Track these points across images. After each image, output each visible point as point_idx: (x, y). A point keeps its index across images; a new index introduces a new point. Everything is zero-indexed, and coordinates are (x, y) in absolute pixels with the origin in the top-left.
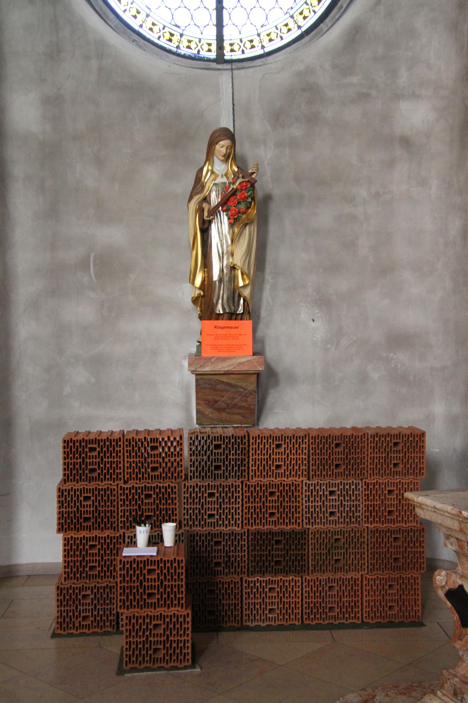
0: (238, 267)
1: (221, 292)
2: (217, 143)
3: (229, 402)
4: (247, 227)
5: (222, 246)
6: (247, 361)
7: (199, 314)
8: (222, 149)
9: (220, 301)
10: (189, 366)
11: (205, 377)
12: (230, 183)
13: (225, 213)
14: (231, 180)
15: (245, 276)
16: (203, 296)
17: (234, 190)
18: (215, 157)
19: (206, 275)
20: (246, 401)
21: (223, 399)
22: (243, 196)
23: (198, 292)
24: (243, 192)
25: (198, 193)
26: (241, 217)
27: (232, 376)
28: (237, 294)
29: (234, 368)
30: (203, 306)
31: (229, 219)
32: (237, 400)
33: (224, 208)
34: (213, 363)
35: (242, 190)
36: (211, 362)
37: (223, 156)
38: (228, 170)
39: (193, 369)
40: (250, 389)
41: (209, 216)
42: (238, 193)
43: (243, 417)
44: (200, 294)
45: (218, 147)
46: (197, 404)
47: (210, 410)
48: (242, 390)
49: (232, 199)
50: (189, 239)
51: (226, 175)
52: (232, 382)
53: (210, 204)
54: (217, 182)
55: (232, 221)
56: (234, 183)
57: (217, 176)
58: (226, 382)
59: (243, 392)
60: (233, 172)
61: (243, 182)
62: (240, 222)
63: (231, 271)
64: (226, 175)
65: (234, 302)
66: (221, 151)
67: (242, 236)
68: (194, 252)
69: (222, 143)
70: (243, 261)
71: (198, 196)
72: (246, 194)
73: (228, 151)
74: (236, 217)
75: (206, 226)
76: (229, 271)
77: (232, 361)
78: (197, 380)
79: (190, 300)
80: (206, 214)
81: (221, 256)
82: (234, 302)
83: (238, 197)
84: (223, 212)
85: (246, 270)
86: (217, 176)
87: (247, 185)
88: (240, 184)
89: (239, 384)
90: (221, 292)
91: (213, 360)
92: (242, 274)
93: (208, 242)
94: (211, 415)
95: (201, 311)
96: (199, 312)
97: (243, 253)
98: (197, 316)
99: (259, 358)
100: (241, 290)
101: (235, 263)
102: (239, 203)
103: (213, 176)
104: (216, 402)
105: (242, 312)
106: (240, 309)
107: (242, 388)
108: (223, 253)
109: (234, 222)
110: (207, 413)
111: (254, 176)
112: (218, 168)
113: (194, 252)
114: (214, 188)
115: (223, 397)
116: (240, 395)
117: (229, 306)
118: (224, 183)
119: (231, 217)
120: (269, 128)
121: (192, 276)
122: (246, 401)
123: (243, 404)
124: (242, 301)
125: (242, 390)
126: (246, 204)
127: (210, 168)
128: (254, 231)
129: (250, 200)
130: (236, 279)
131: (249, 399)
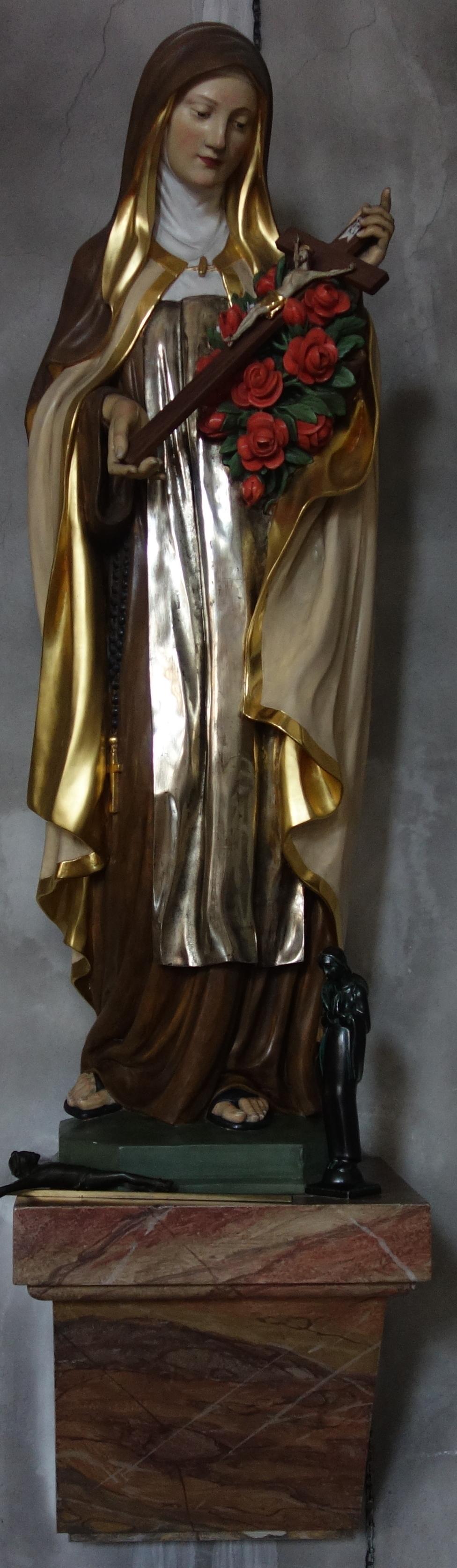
0: (287, 722)
1: (195, 855)
2: (180, 94)
3: (229, 1428)
4: (333, 525)
5: (199, 616)
6: (341, 1232)
7: (76, 967)
8: (206, 126)
9: (188, 903)
10: (17, 1257)
11: (101, 1311)
12: (242, 301)
13: (215, 449)
14: (247, 286)
15: (319, 773)
16: (95, 878)
17: (266, 326)
18: (169, 180)
19: (115, 766)
20: (320, 1424)
21: (198, 1416)
22: (315, 354)
23: (70, 853)
24: (317, 333)
25: (79, 355)
26: (303, 466)
27: (256, 1307)
28: (274, 867)
29: (268, 1269)
30: (95, 927)
31: (235, 479)
32: (275, 1420)
33: (215, 420)
34: (149, 1242)
35: (307, 326)
36: (140, 1237)
37: (211, 163)
38: (232, 239)
39: (45, 1274)
40: (345, 1367)
41: (132, 456)
42: (290, 346)
43: (299, 1496)
44: (79, 864)
45: (184, 114)
46: (61, 1438)
47: (131, 1468)
48: (300, 1374)
49: (255, 372)
50: (34, 596)
51: (223, 263)
52: (252, 1336)
53: (142, 402)
54: (175, 293)
55: (254, 487)
56: (264, 294)
57: (177, 266)
58: (218, 1338)
59: (308, 1385)
60: (261, 249)
61: (316, 282)
62: (297, 492)
63: (245, 750)
64: (223, 263)
65: (258, 906)
66: (197, 136)
67: (303, 568)
68: (55, 652)
69: (206, 90)
70: (309, 693)
71: (78, 369)
72: (331, 346)
73: (237, 137)
74: (273, 466)
75: (117, 517)
76: (233, 748)
77: (255, 1232)
78: (59, 1328)
79: (32, 891)
80: (118, 445)
81: (196, 664)
82: (258, 906)
83: (288, 364)
84: (208, 442)
85: (324, 740)
86: (177, 266)
87: (335, 303)
88: (297, 294)
89: (288, 1345)
90: (195, 855)
91: (151, 1224)
92: (305, 760)
93: (125, 600)
94: (131, 1492)
95: (86, 950)
96: (76, 958)
97: (308, 653)
98: (68, 970)
99: (402, 1217)
100: (298, 844)
101: (267, 700)
102: (292, 393)
103: (156, 269)
104: (165, 1429)
105: (298, 957)
106: (289, 945)
107: (300, 1364)
108: (204, 650)
109: (265, 497)
110: (112, 1478)
111: (372, 257)
112: (180, 232)
113: (55, 652)
114: (162, 320)
115: (199, 1405)
116: (289, 1400)
117: (235, 930)
118: (214, 302)
119: (251, 466)
120: (425, 90)
121: (40, 771)
122: (320, 1424)
123: (304, 1440)
124: (299, 904)
125: (300, 1374)
126: (328, 402)
127: (141, 223)
128: (364, 540)
129: (347, 379)
130: (271, 790)
131: (334, 1418)
